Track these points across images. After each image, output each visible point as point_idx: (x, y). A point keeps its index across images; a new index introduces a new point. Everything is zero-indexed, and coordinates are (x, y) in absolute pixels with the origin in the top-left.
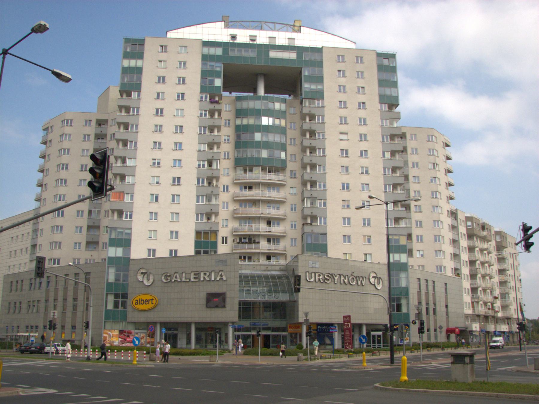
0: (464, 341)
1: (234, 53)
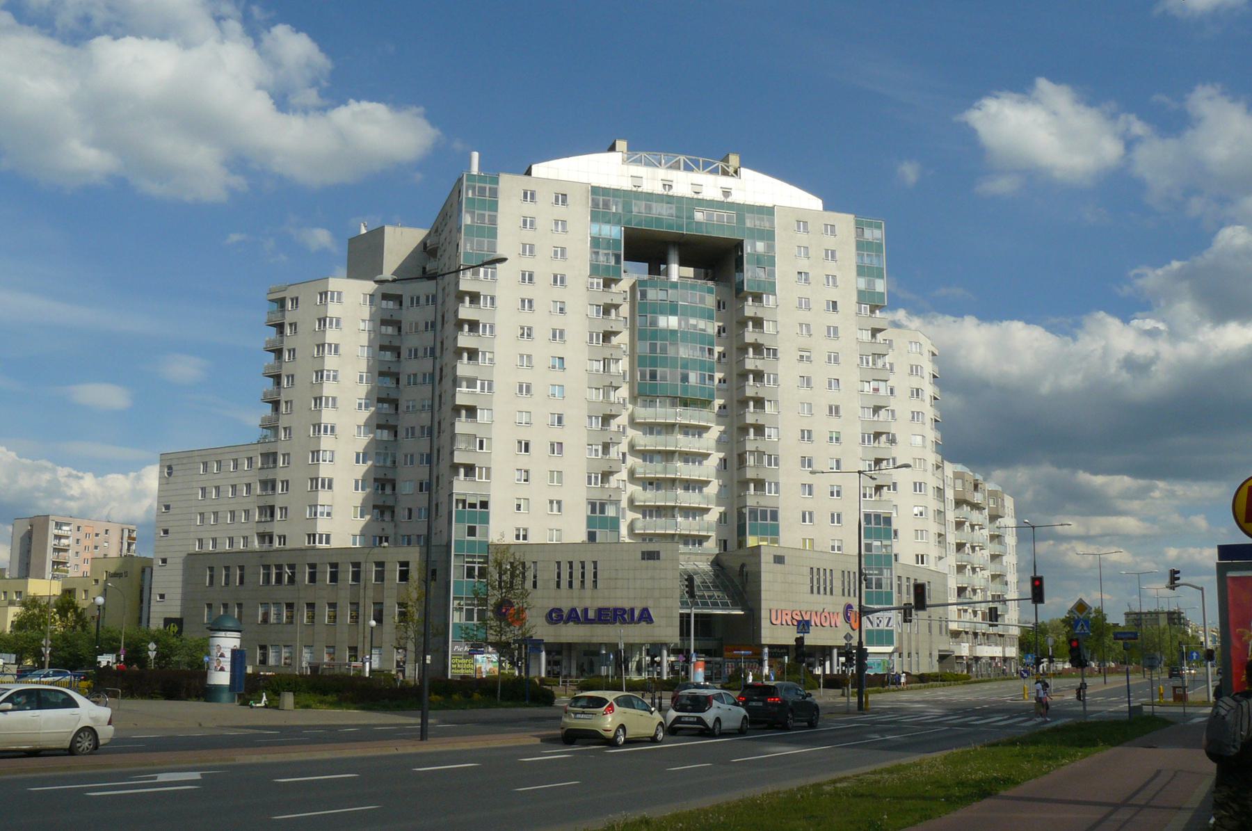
0: (105, 660)
1: (638, 208)
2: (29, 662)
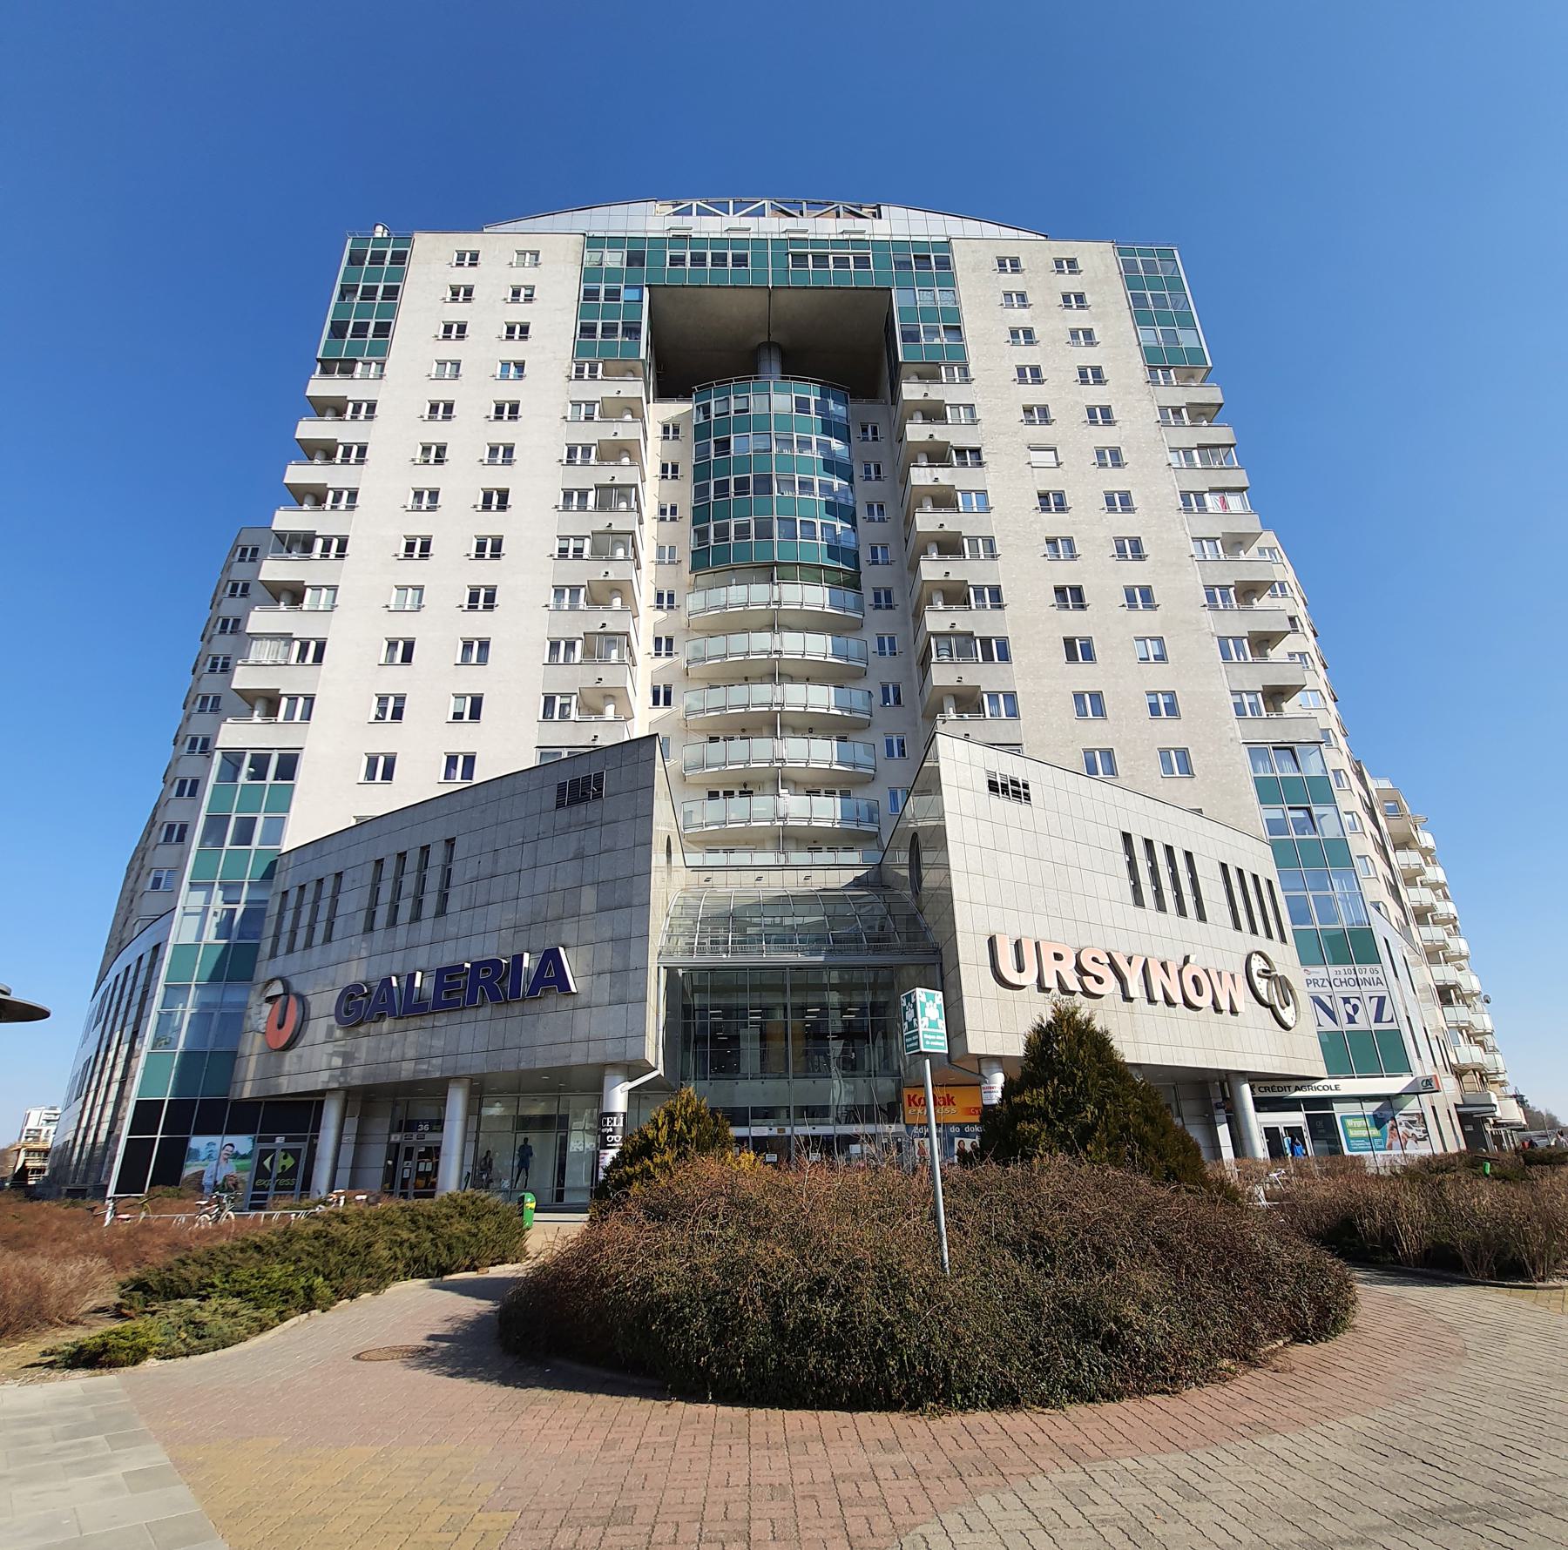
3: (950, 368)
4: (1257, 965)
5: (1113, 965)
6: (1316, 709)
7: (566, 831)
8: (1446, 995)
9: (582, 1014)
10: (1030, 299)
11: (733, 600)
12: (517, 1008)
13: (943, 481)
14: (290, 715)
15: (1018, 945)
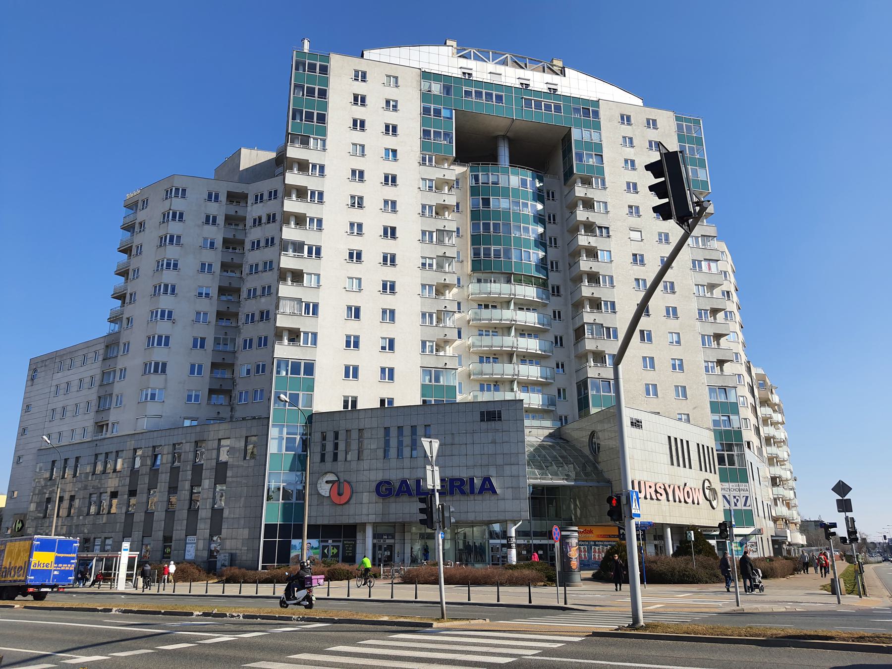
2: (524, 552)
3: (597, 178)
4: (707, 484)
5: (665, 489)
6: (733, 343)
7: (487, 431)
8: (775, 481)
9: (501, 503)
10: (635, 142)
11: (493, 290)
12: (472, 497)
13: (593, 244)
14: (306, 342)
15: (639, 483)
